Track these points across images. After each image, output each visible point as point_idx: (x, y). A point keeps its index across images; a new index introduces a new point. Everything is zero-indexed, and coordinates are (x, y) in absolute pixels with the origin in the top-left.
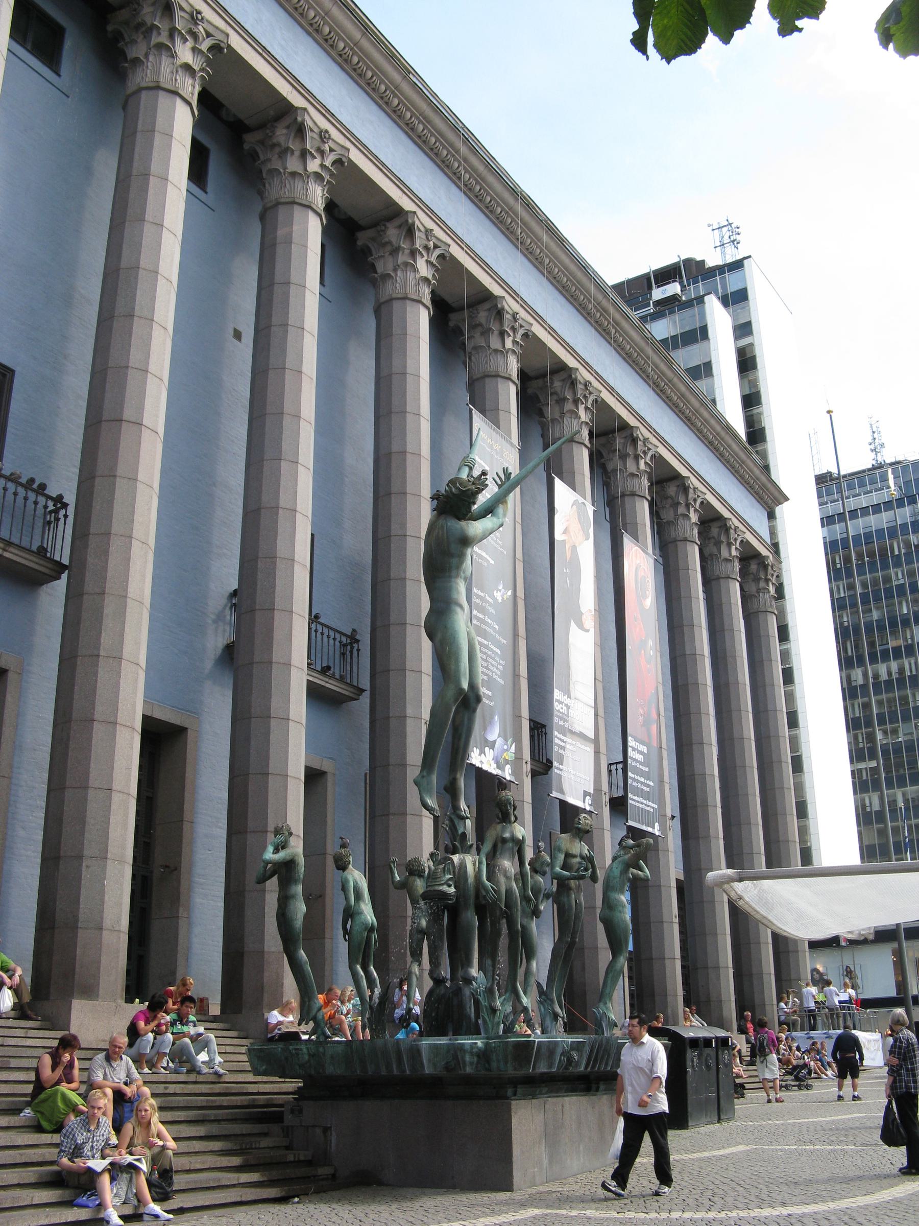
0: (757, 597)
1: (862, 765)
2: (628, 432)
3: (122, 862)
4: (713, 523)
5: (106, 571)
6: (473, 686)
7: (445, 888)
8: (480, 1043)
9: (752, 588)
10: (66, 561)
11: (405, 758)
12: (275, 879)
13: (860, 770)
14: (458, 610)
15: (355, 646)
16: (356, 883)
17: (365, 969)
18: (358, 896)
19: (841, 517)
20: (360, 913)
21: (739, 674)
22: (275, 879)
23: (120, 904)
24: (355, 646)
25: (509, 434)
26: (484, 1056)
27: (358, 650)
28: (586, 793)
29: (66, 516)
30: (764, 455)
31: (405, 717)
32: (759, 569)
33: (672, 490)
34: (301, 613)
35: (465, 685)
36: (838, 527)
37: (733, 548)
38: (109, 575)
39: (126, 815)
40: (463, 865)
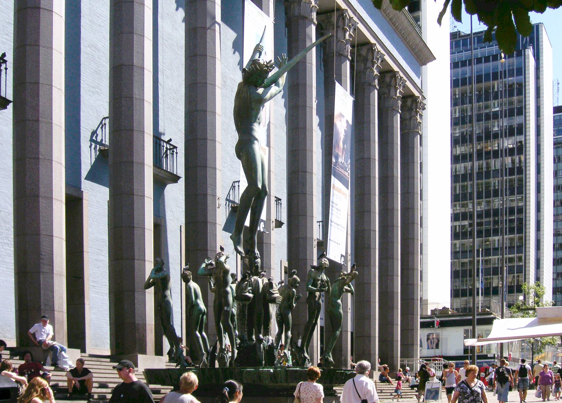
0: (364, 73)
1: (457, 223)
2: (340, 12)
3: (61, 275)
4: (388, 76)
5: (39, 107)
6: (263, 185)
7: (247, 294)
8: (272, 371)
9: (407, 116)
10: (10, 97)
11: (207, 219)
12: (152, 288)
13: (456, 226)
14: (256, 142)
15: (175, 150)
16: (195, 290)
17: (201, 333)
18: (197, 297)
19: (464, 64)
20: (198, 305)
21: (395, 171)
22: (152, 288)
23: (62, 298)
24: (175, 150)
25: (268, 14)
26: (274, 377)
27: (177, 153)
28: (342, 256)
29: (6, 69)
30: (417, 19)
31: (206, 194)
32: (412, 105)
33: (364, 52)
34: (149, 133)
35: (260, 186)
36: (460, 70)
37: (398, 91)
38: (41, 109)
39: (62, 249)
40: (257, 282)
